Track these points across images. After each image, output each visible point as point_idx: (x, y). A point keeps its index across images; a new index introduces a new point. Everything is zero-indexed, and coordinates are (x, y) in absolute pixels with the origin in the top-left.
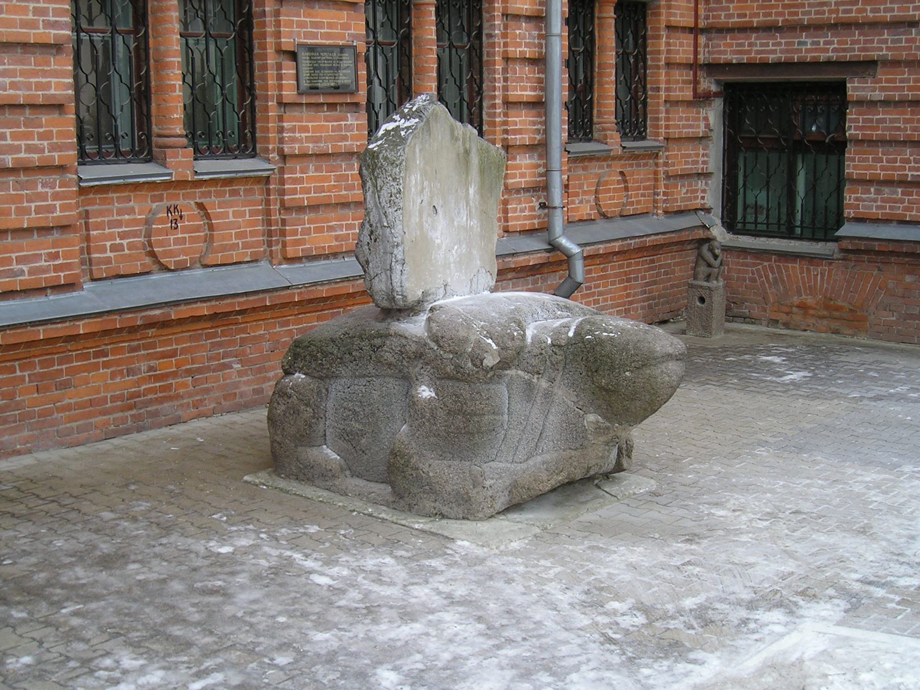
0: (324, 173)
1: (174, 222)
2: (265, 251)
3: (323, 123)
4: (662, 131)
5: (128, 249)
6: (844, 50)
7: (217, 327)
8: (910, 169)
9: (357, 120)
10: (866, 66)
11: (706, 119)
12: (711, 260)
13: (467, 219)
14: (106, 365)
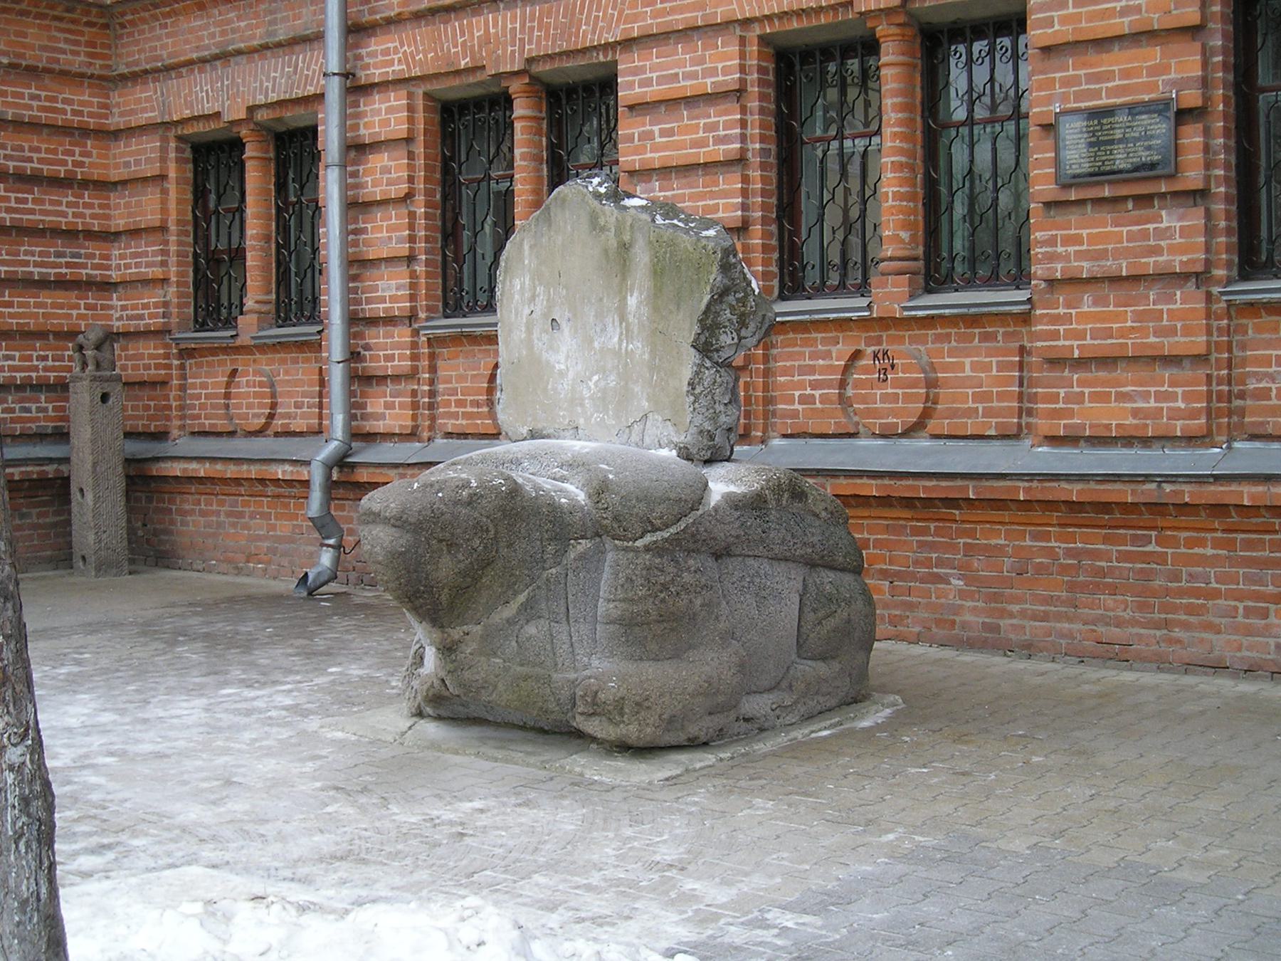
0: (1111, 308)
1: (883, 372)
3: (1109, 229)
5: (821, 403)
9: (1180, 219)
13: (620, 340)
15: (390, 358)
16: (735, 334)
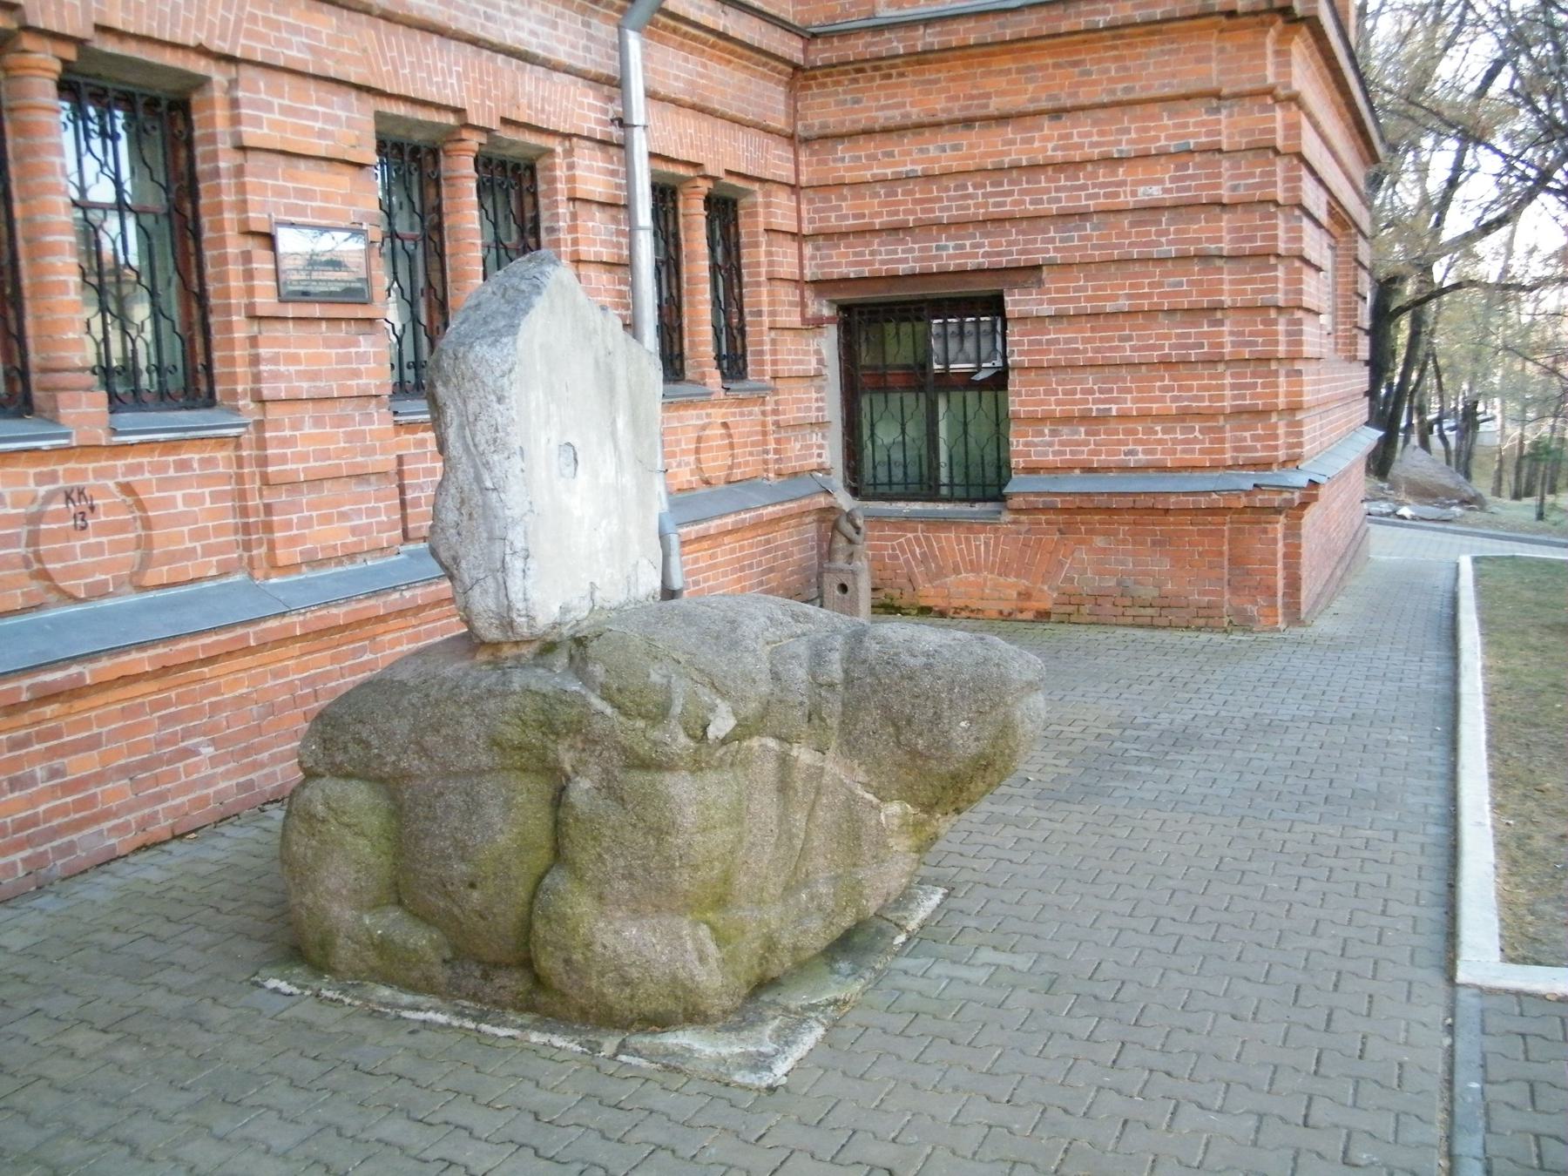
2: (240, 558)
4: (768, 368)
6: (999, 254)
7: (168, 689)
8: (1095, 402)
10: (1030, 273)
11: (818, 352)
12: (853, 535)
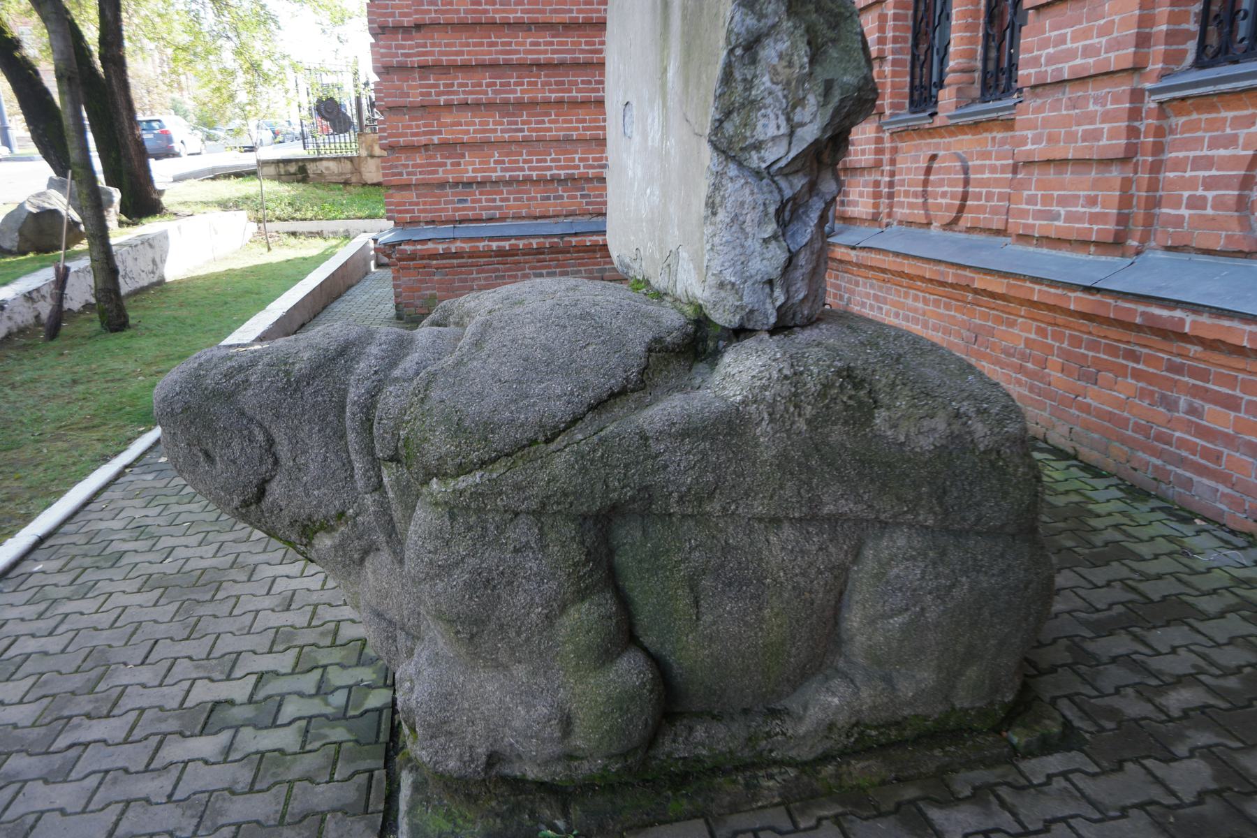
5: (1213, 208)
14: (1137, 375)
15: (863, 152)
16: (782, 119)
